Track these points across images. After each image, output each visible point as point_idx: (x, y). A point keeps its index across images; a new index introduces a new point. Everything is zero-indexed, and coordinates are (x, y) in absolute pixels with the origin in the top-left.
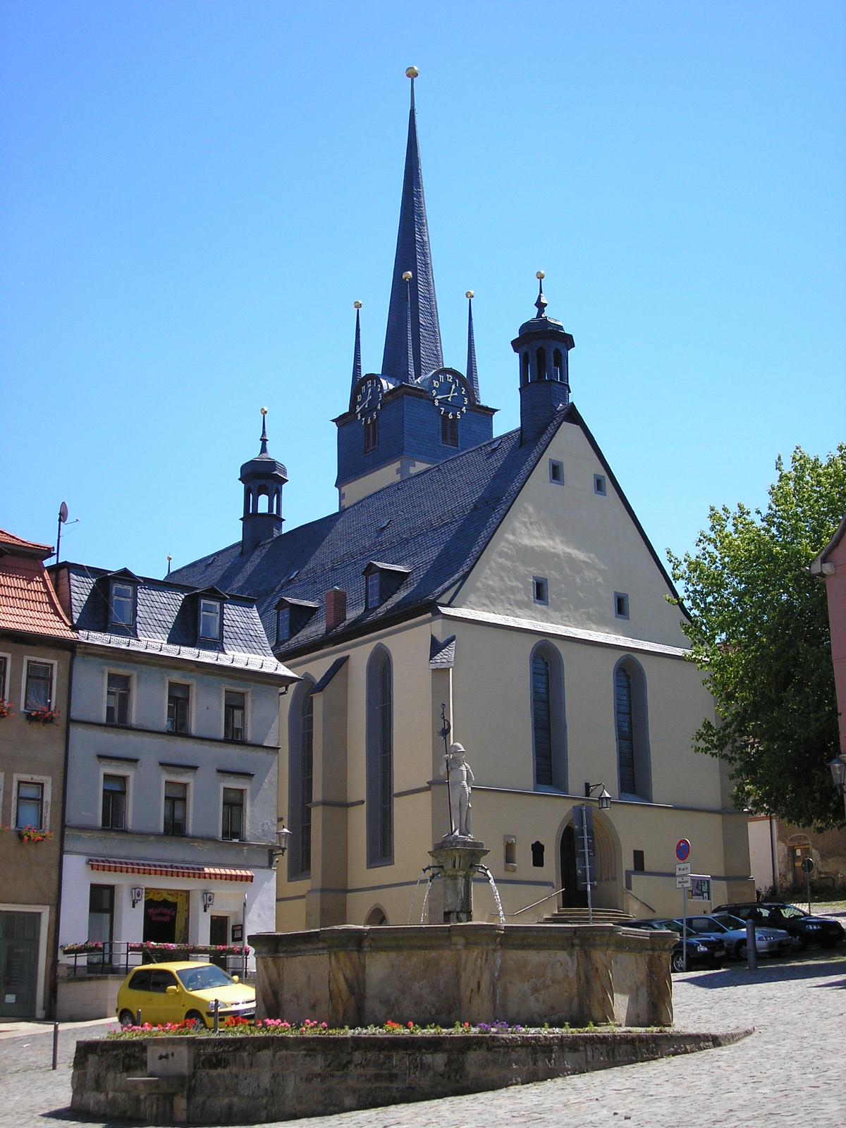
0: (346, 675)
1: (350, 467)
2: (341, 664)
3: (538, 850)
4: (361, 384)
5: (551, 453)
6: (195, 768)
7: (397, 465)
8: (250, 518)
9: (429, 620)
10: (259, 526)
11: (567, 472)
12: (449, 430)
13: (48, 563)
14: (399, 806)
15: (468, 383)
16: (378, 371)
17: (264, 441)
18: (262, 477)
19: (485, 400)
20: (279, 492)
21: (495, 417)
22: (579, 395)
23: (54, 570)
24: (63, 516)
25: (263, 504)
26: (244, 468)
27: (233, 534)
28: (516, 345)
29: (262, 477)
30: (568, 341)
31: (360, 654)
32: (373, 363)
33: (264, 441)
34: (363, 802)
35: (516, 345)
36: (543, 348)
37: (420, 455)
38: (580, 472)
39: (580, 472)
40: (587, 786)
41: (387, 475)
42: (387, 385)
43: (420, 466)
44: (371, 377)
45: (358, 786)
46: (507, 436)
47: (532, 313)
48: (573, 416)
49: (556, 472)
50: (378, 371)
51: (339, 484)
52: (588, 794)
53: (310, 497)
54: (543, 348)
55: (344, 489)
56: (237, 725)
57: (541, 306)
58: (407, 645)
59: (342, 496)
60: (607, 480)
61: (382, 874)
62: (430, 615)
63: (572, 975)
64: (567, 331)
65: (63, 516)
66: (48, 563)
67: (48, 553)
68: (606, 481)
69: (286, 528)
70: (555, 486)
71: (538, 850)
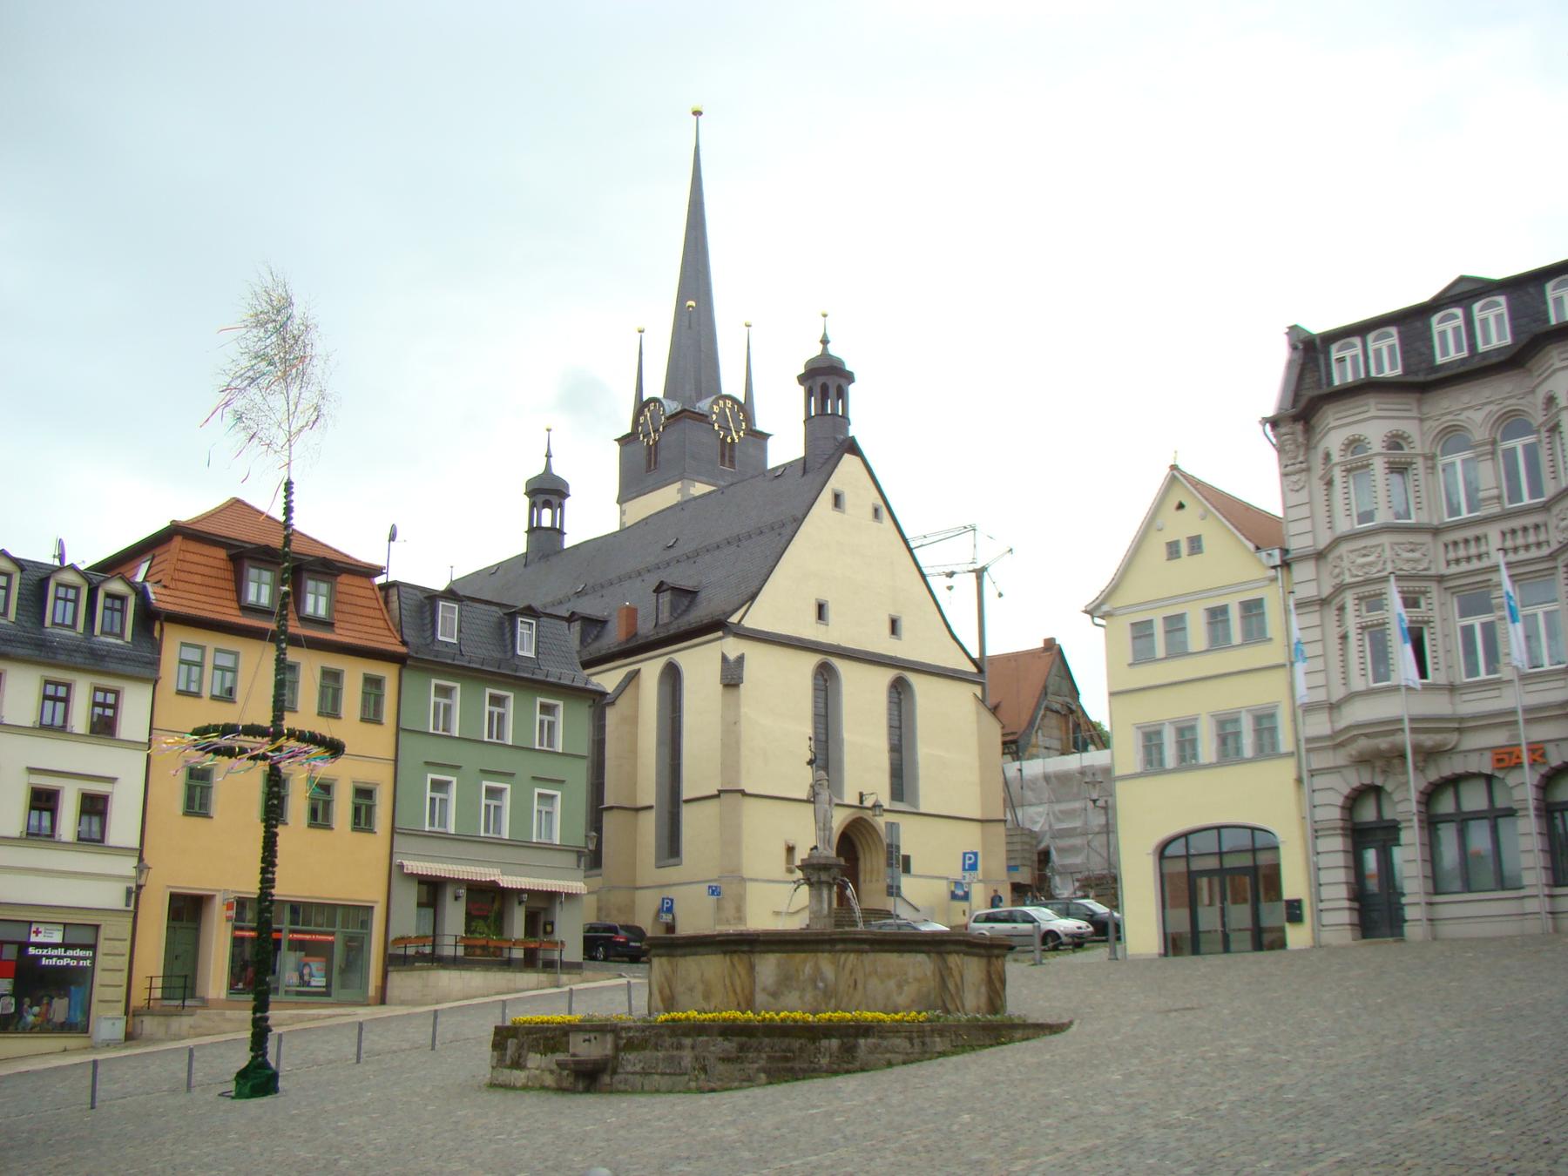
0: (638, 686)
1: (632, 485)
2: (633, 677)
3: (319, 815)
4: (642, 406)
5: (834, 483)
6: (512, 775)
7: (678, 485)
8: (534, 531)
9: (720, 638)
10: (544, 541)
11: (848, 500)
12: (727, 452)
13: (380, 580)
14: (687, 813)
15: (745, 409)
16: (660, 394)
17: (549, 456)
18: (547, 491)
19: (760, 425)
20: (561, 506)
21: (770, 441)
22: (857, 430)
23: (383, 587)
24: (392, 537)
25: (546, 518)
26: (529, 483)
27: (516, 544)
28: (802, 379)
29: (547, 491)
30: (849, 377)
31: (651, 669)
32: (655, 387)
33: (549, 456)
34: (650, 807)
35: (802, 379)
36: (826, 380)
37: (697, 477)
38: (860, 498)
39: (860, 498)
40: (861, 795)
41: (668, 496)
42: (672, 407)
43: (699, 489)
44: (654, 400)
45: (648, 791)
46: (786, 467)
47: (817, 350)
48: (853, 448)
49: (837, 499)
50: (660, 394)
51: (621, 500)
52: (861, 801)
53: (592, 514)
54: (826, 380)
55: (627, 506)
56: (62, 658)
57: (825, 342)
58: (700, 664)
59: (623, 513)
60: (884, 510)
61: (671, 874)
62: (720, 634)
63: (929, 973)
64: (848, 368)
65: (392, 537)
66: (380, 580)
67: (378, 571)
68: (883, 509)
69: (569, 542)
70: (836, 514)
71: (319, 815)
